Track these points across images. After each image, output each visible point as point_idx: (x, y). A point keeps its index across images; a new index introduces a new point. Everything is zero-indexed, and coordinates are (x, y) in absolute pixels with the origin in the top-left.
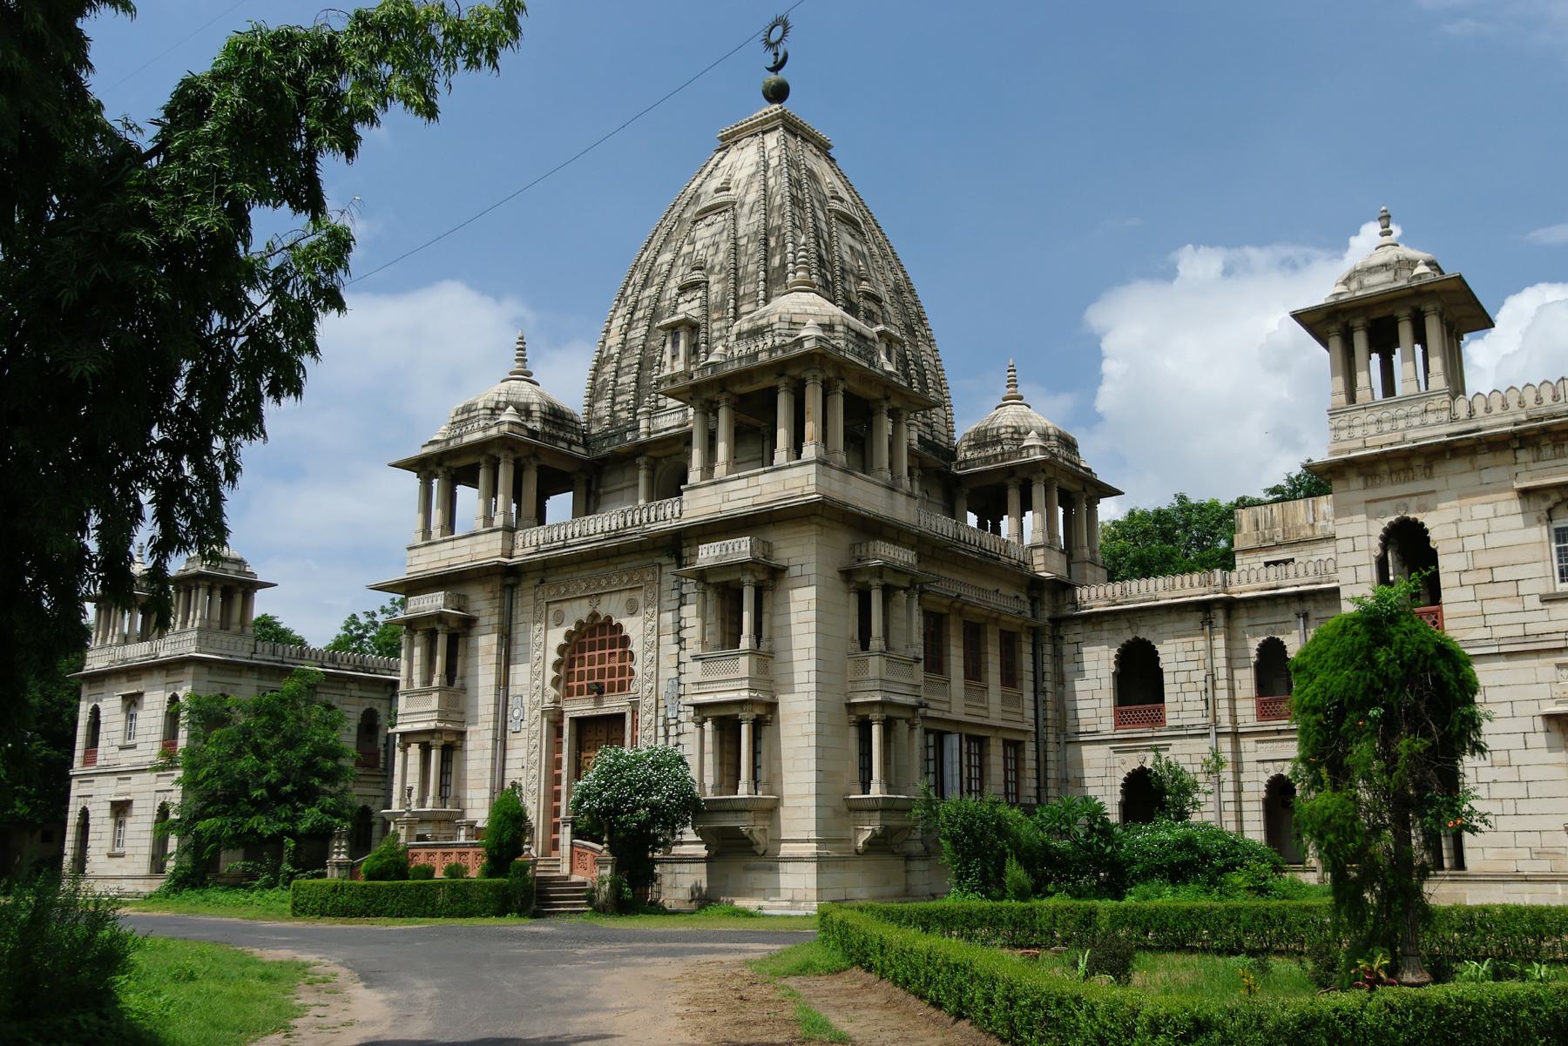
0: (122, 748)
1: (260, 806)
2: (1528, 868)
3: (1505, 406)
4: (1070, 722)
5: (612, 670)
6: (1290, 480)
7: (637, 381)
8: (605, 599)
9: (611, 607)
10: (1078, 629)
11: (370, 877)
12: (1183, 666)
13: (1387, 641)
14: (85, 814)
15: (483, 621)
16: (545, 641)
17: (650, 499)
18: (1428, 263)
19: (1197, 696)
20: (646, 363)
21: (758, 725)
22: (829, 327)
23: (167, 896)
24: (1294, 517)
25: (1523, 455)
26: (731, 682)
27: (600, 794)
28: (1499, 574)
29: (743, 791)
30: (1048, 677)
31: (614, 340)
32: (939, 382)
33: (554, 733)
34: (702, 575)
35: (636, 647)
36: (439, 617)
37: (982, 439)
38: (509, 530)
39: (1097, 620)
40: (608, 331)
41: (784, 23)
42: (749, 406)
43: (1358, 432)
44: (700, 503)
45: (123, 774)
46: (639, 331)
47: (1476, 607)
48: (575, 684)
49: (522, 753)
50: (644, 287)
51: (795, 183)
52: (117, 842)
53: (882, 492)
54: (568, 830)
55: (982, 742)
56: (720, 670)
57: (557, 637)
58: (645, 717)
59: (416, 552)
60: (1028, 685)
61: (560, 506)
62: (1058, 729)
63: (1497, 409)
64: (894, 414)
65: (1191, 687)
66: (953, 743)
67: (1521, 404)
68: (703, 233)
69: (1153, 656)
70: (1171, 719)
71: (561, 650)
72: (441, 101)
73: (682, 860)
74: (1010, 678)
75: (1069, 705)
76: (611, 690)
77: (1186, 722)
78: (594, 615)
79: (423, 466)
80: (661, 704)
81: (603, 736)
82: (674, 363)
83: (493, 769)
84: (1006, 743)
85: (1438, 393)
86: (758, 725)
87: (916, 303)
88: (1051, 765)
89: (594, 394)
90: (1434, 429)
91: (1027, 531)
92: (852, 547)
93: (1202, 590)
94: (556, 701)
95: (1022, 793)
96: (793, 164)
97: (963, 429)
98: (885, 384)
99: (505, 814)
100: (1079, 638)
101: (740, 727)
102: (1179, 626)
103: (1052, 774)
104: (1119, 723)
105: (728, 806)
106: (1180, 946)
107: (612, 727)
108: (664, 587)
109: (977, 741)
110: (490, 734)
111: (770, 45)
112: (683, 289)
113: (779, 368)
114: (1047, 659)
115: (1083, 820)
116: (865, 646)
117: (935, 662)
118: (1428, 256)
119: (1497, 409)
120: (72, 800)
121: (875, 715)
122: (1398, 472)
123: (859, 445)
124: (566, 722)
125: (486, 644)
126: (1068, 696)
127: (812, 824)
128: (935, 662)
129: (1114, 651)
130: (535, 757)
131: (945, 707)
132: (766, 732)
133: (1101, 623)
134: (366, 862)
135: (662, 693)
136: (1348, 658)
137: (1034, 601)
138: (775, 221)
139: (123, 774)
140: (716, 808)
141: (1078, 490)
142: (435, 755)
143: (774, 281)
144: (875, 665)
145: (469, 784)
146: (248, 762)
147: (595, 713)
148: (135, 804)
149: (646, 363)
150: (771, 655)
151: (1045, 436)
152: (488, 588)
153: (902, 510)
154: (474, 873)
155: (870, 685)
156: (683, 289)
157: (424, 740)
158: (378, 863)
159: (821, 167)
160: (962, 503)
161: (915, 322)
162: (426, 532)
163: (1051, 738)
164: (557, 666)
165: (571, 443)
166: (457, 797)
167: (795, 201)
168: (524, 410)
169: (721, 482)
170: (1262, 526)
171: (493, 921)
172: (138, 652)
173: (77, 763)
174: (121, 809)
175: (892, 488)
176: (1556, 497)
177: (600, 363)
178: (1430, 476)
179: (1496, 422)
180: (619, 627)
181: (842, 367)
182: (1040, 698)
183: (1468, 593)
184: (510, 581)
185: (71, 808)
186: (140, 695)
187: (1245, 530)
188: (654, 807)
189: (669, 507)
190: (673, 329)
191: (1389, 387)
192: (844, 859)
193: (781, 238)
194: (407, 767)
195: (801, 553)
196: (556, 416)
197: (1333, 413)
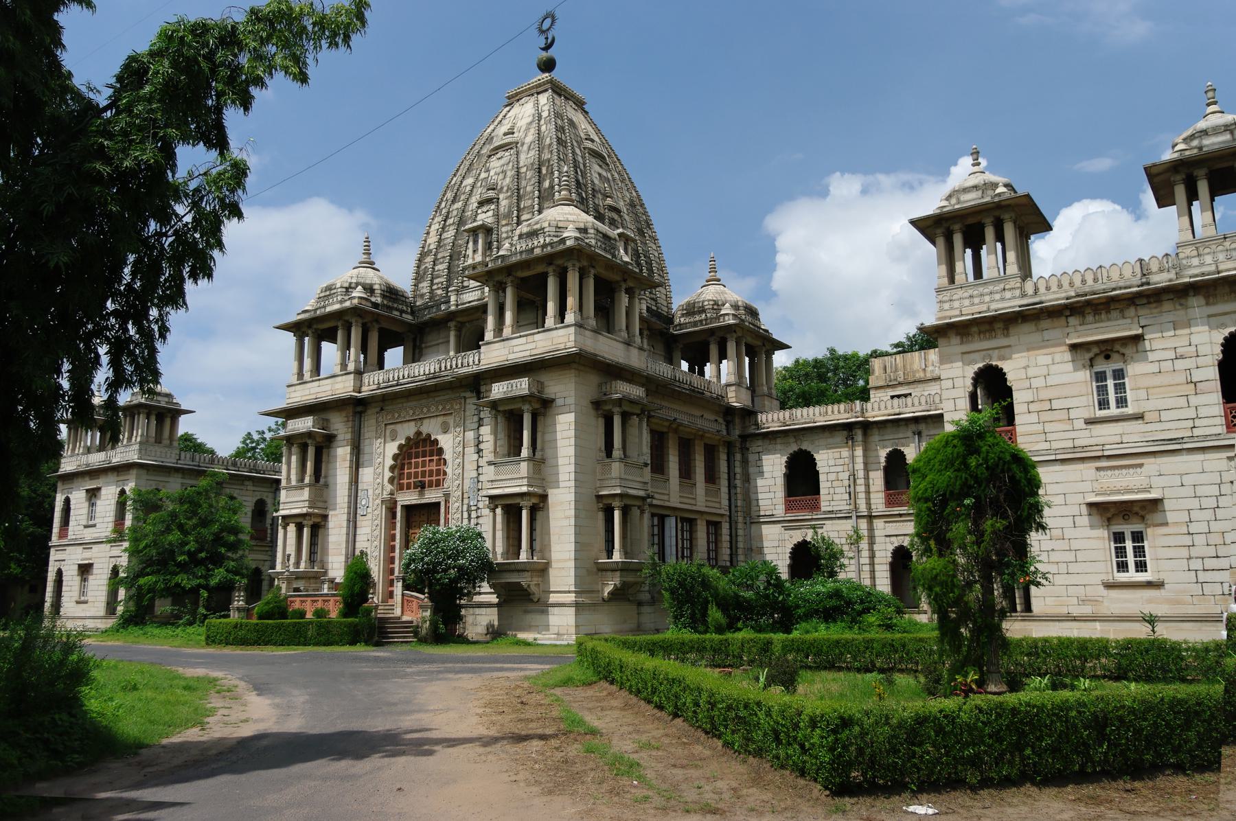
0: (86, 527)
1: (183, 567)
2: (1076, 611)
3: (1060, 286)
4: (754, 509)
5: (431, 472)
6: (909, 338)
7: (449, 268)
8: (426, 422)
9: (430, 427)
10: (760, 443)
11: (260, 618)
12: (832, 469)
13: (977, 451)
14: (60, 573)
15: (340, 437)
16: (384, 451)
17: (458, 351)
18: (1006, 186)
19: (843, 490)
20: (455, 256)
22: (584, 230)
24: (911, 364)
25: (1072, 321)
26: (515, 480)
28: (1055, 404)
29: (524, 557)
30: (738, 476)
31: (432, 240)
33: (390, 515)
34: (494, 405)
35: (448, 455)
36: (309, 434)
38: (359, 373)
39: (773, 437)
40: (428, 233)
42: (527, 285)
43: (956, 304)
44: (493, 354)
45: (87, 545)
46: (450, 233)
47: (1039, 427)
48: (405, 481)
49: (368, 530)
50: (454, 202)
52: (83, 592)
54: (400, 584)
55: (691, 522)
56: (507, 472)
57: (392, 448)
58: (455, 505)
60: (724, 483)
61: (394, 356)
62: (746, 514)
63: (1054, 288)
64: (630, 292)
65: (839, 483)
66: (671, 523)
67: (1071, 284)
68: (495, 164)
69: (812, 462)
70: (825, 506)
71: (395, 457)
72: (311, 71)
74: (711, 477)
75: (753, 496)
76: (430, 486)
77: (835, 509)
78: (419, 433)
79: (298, 328)
81: (424, 518)
82: (474, 256)
83: (347, 542)
84: (709, 523)
85: (1013, 277)
86: (534, 510)
87: (645, 213)
89: (419, 278)
90: (1010, 302)
91: (723, 374)
92: (600, 385)
93: (847, 415)
94: (392, 494)
96: (558, 115)
97: (678, 302)
98: (623, 270)
100: (760, 449)
102: (830, 441)
103: (741, 545)
104: (789, 508)
105: (513, 567)
106: (831, 666)
107: (430, 512)
108: (468, 413)
109: (688, 521)
111: (542, 32)
112: (481, 204)
113: (549, 259)
114: (737, 464)
115: (763, 577)
117: (658, 466)
118: (1005, 180)
119: (1054, 288)
121: (616, 503)
122: (985, 332)
123: (605, 314)
124: (399, 509)
125: (342, 453)
126: (752, 490)
127: (572, 580)
128: (658, 466)
129: (785, 459)
130: (377, 533)
131: (666, 497)
132: (539, 515)
133: (775, 439)
134: (258, 607)
135: (466, 488)
136: (949, 463)
137: (728, 424)
138: (546, 156)
139: (87, 545)
140: (504, 569)
141: (759, 345)
142: (306, 531)
143: (545, 198)
144: (616, 468)
146: (174, 537)
148: (95, 566)
149: (455, 256)
151: (735, 307)
152: (344, 414)
153: (635, 359)
154: (334, 615)
155: (613, 482)
156: (481, 204)
157: (299, 521)
159: (578, 118)
160: (677, 354)
161: (644, 227)
162: (300, 374)
163: (740, 519)
164: (392, 469)
165: (402, 312)
166: (322, 561)
168: (369, 289)
170: (888, 370)
171: (347, 649)
172: (97, 459)
173: (54, 537)
174: (85, 570)
175: (628, 344)
176: (1095, 350)
177: (423, 255)
178: (1007, 335)
179: (1053, 298)
180: (436, 441)
181: (593, 258)
182: (733, 491)
183: (1034, 418)
185: (50, 569)
186: (99, 489)
187: (877, 373)
189: (471, 357)
190: (474, 232)
191: (978, 273)
193: (550, 167)
194: (287, 540)
196: (391, 293)
197: (939, 291)
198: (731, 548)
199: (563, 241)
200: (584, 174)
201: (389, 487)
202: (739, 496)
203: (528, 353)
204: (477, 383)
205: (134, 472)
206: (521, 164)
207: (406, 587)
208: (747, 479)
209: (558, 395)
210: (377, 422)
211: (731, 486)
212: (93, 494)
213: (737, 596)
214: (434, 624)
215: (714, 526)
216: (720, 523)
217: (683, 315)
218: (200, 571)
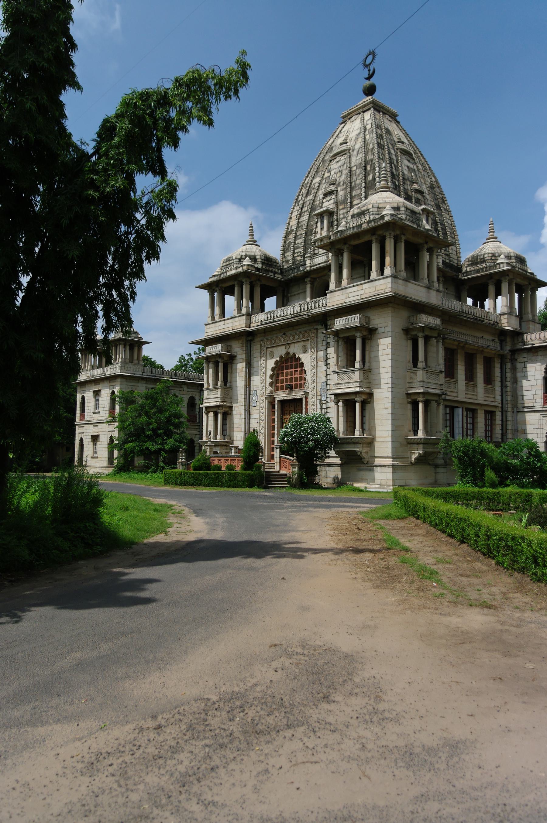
1: (149, 438)
7: (305, 242)
8: (292, 346)
9: (295, 349)
10: (525, 355)
11: (195, 469)
14: (81, 440)
15: (239, 357)
17: (312, 298)
20: (309, 232)
21: (364, 404)
22: (397, 209)
23: (115, 475)
26: (351, 383)
27: (292, 435)
29: (357, 434)
31: (294, 223)
32: (453, 233)
34: (337, 333)
35: (307, 368)
36: (220, 355)
37: (475, 261)
38: (249, 315)
39: (535, 351)
40: (290, 218)
41: (373, 53)
42: (357, 251)
44: (335, 299)
46: (305, 217)
48: (280, 385)
49: (257, 416)
50: (307, 195)
51: (380, 137)
52: (95, 452)
53: (424, 290)
56: (346, 378)
57: (271, 363)
58: (312, 400)
59: (208, 326)
60: (498, 384)
61: (271, 303)
64: (430, 251)
66: (459, 412)
68: (334, 166)
71: (273, 369)
73: (330, 465)
74: (489, 380)
75: (519, 393)
78: (288, 353)
79: (210, 287)
80: (319, 394)
81: (292, 408)
82: (321, 232)
83: (245, 423)
84: (486, 412)
86: (364, 404)
87: (441, 193)
88: (509, 423)
89: (285, 249)
94: (272, 393)
95: (494, 436)
96: (378, 127)
98: (425, 235)
99: (251, 443)
100: (525, 360)
101: (356, 404)
103: (509, 427)
105: (350, 441)
108: (319, 339)
109: (471, 411)
110: (243, 408)
111: (366, 66)
112: (326, 195)
113: (373, 231)
114: (508, 370)
116: (415, 365)
117: (450, 372)
120: (76, 435)
121: (420, 399)
123: (412, 268)
124: (276, 402)
125: (240, 367)
127: (390, 450)
128: (450, 372)
130: (263, 418)
131: (455, 394)
132: (368, 407)
135: (319, 389)
137: (502, 342)
138: (370, 157)
139: (95, 424)
140: (344, 442)
143: (370, 187)
144: (420, 375)
145: (235, 430)
146: (143, 419)
147: (289, 398)
148: (100, 436)
149: (309, 232)
150: (370, 370)
151: (509, 257)
152: (240, 342)
153: (434, 298)
154: (238, 469)
156: (326, 195)
157: (215, 410)
158: (198, 463)
161: (440, 202)
162: (213, 317)
166: (230, 435)
167: (380, 146)
168: (254, 259)
169: (345, 288)
171: (247, 490)
172: (98, 373)
173: (77, 419)
174: (95, 438)
177: (288, 234)
180: (299, 358)
182: (504, 390)
184: (249, 338)
185: (76, 438)
186: (100, 391)
188: (316, 441)
189: (321, 301)
190: (321, 215)
192: (405, 466)
193: (373, 165)
194: (209, 422)
195: (384, 321)
196: (268, 261)
198: (502, 429)
199: (382, 217)
200: (397, 168)
201: (270, 389)
202: (509, 393)
203: (359, 297)
204: (325, 319)
205: (119, 380)
206: (353, 164)
207: (282, 452)
208: (515, 381)
209: (380, 326)
210: (261, 346)
211: (503, 386)
212: (97, 394)
213: (506, 463)
214: (300, 476)
215: (490, 414)
216: (477, 409)
217: (469, 265)
218: (159, 441)
